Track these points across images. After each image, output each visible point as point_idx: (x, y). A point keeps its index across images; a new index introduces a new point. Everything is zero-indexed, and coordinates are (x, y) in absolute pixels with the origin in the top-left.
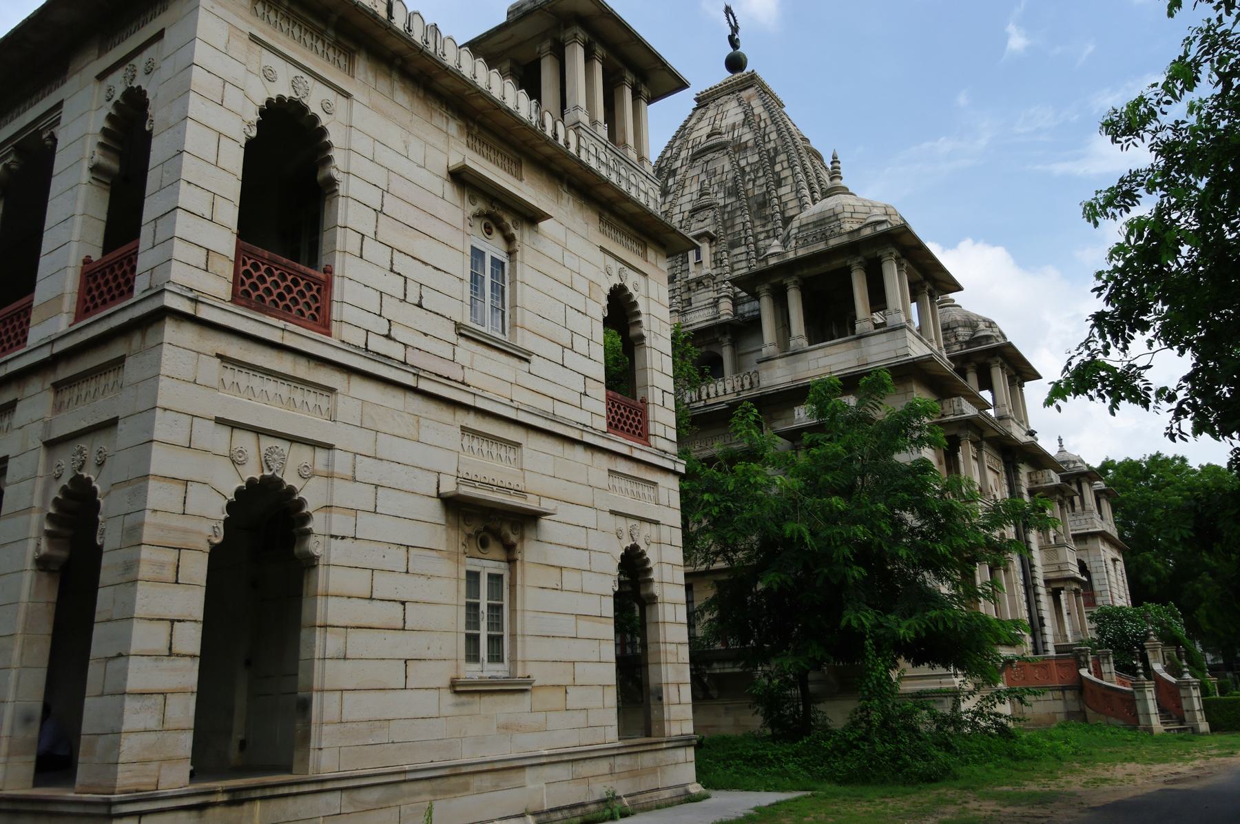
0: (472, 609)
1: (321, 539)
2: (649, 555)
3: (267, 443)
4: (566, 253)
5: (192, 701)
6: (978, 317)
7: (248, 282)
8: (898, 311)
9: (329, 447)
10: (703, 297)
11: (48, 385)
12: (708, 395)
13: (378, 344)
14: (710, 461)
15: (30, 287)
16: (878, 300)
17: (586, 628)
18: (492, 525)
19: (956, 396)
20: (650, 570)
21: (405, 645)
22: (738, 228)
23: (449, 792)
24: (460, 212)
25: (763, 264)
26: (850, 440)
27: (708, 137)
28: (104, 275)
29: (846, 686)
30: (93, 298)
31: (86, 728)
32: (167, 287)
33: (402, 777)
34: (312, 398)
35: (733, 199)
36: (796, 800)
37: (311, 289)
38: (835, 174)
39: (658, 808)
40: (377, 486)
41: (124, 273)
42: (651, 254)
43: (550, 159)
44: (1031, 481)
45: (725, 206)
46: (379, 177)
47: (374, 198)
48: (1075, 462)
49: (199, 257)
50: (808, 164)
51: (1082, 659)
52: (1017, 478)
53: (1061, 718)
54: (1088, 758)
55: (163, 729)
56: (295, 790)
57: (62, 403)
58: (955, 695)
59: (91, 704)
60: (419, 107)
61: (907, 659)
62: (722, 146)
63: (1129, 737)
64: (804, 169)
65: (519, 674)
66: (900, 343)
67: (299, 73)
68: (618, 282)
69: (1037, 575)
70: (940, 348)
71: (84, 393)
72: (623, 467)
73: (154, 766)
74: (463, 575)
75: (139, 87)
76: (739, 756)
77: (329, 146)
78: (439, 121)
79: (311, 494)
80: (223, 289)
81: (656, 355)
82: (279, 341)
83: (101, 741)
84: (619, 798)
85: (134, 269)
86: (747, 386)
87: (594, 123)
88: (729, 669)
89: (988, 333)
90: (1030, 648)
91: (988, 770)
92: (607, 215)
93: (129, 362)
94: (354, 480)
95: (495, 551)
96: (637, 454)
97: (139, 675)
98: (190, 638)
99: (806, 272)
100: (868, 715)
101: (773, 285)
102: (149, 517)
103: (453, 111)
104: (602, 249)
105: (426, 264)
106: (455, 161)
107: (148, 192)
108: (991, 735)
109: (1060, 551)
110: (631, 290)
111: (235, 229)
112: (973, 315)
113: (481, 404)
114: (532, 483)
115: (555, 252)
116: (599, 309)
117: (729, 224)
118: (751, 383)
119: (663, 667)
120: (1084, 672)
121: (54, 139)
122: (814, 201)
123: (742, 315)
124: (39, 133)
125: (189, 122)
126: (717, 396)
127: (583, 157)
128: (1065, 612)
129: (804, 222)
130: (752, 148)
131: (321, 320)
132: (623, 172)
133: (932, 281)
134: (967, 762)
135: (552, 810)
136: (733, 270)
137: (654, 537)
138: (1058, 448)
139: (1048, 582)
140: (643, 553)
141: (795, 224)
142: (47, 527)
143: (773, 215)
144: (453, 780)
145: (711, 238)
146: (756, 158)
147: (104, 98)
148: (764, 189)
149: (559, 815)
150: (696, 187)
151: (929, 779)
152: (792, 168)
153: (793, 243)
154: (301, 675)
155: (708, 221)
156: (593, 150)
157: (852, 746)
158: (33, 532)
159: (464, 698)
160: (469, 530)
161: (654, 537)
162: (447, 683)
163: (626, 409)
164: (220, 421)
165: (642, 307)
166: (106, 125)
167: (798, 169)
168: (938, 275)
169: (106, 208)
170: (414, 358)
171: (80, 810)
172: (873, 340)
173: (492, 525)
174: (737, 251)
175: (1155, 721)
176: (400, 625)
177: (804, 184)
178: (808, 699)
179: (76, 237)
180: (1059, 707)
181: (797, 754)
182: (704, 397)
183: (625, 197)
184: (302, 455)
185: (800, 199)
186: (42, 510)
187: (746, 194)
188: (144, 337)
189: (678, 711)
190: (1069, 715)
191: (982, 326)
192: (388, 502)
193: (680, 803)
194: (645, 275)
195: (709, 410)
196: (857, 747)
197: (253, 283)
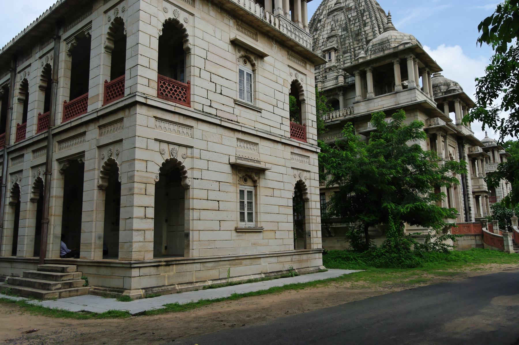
0: (242, 203)
1: (190, 179)
2: (306, 184)
3: (172, 147)
4: (275, 69)
5: (152, 233)
6: (451, 81)
7: (162, 89)
8: (413, 82)
9: (192, 147)
10: (332, 75)
11: (96, 127)
12: (333, 117)
13: (207, 109)
14: (332, 145)
15: (87, 90)
16: (405, 76)
17: (283, 210)
18: (248, 173)
19: (437, 117)
20: (307, 189)
21: (220, 216)
22: (347, 45)
23: (236, 265)
24: (235, 56)
25: (357, 62)
26: (390, 136)
27: (335, 4)
28: (113, 87)
29: (383, 233)
30: (109, 96)
31: (120, 241)
32: (137, 94)
33: (220, 259)
34: (185, 130)
35: (345, 32)
36: (359, 272)
37: (183, 90)
38: (389, 21)
39: (308, 273)
40: (208, 161)
41: (120, 87)
42: (308, 66)
43: (268, 31)
44: (469, 151)
45: (342, 36)
46: (205, 45)
47: (203, 54)
48: (492, 142)
49: (146, 82)
50: (378, 16)
51: (484, 224)
52: (463, 150)
53: (473, 246)
54: (476, 261)
55: (145, 241)
56: (186, 262)
57: (102, 133)
58: (428, 237)
59: (122, 233)
60: (219, 16)
61: (408, 223)
62: (341, 9)
63: (499, 254)
64: (376, 18)
65: (259, 226)
66: (413, 95)
67: (176, 8)
68: (295, 79)
69: (469, 190)
70: (431, 96)
71: (109, 130)
72: (296, 151)
73: (143, 253)
74: (239, 192)
75: (120, 17)
76: (340, 257)
77: (187, 35)
78: (226, 21)
79: (187, 164)
80: (154, 93)
81: (309, 107)
82: (173, 110)
83: (126, 245)
84: (294, 269)
85: (124, 86)
86: (349, 113)
87: (285, 14)
88: (339, 225)
89: (455, 88)
90: (464, 220)
91: (435, 264)
92: (290, 52)
93: (125, 120)
94: (201, 159)
95: (249, 183)
96: (302, 146)
97: (137, 224)
98: (151, 213)
99: (375, 65)
100: (390, 243)
101: (361, 71)
102: (136, 173)
103: (231, 16)
104: (289, 66)
105: (223, 78)
106: (232, 37)
107: (127, 58)
108: (440, 252)
109: (480, 180)
110: (300, 81)
111: (157, 71)
112: (448, 80)
113: (244, 129)
114: (262, 158)
115: (270, 69)
116: (287, 90)
117: (343, 43)
118: (350, 112)
119: (311, 224)
120: (484, 229)
121: (90, 36)
122: (380, 33)
123: (348, 83)
124: (83, 32)
125: (140, 32)
126: (336, 117)
127: (281, 30)
128: (481, 205)
129: (374, 43)
130: (354, 9)
131: (187, 101)
132: (297, 33)
133: (428, 67)
134: (427, 261)
135: (270, 273)
136: (344, 64)
137: (308, 177)
138: (485, 136)
139: (474, 193)
140: (304, 183)
141: (371, 44)
142: (101, 175)
143: (362, 39)
144: (237, 261)
145: (335, 50)
146: (355, 14)
147: (107, 21)
148: (359, 27)
149: (273, 274)
150: (329, 27)
151: (411, 267)
152: (371, 18)
153: (370, 53)
154: (185, 225)
155: (334, 42)
156: (285, 26)
157: (382, 254)
158: (96, 177)
159: (240, 234)
160: (240, 175)
161: (308, 177)
162: (234, 229)
163: (298, 131)
164: (156, 140)
165: (304, 88)
166: (109, 31)
167: (373, 18)
168: (432, 65)
169: (110, 62)
170: (220, 114)
171: (121, 265)
172: (402, 94)
173: (248, 173)
174: (346, 55)
175: (512, 249)
176: (218, 209)
177: (376, 25)
178: (368, 237)
179: (101, 73)
180: (473, 242)
181: (361, 257)
182: (331, 118)
183: (298, 45)
184: (183, 150)
185: (374, 32)
186: (98, 169)
187: (351, 30)
188: (129, 111)
189: (316, 240)
190: (477, 245)
191: (452, 85)
192: (213, 166)
193: (317, 272)
194: (306, 75)
195: (332, 123)
196: (385, 255)
197: (162, 85)
